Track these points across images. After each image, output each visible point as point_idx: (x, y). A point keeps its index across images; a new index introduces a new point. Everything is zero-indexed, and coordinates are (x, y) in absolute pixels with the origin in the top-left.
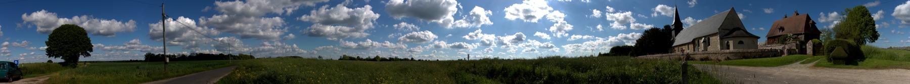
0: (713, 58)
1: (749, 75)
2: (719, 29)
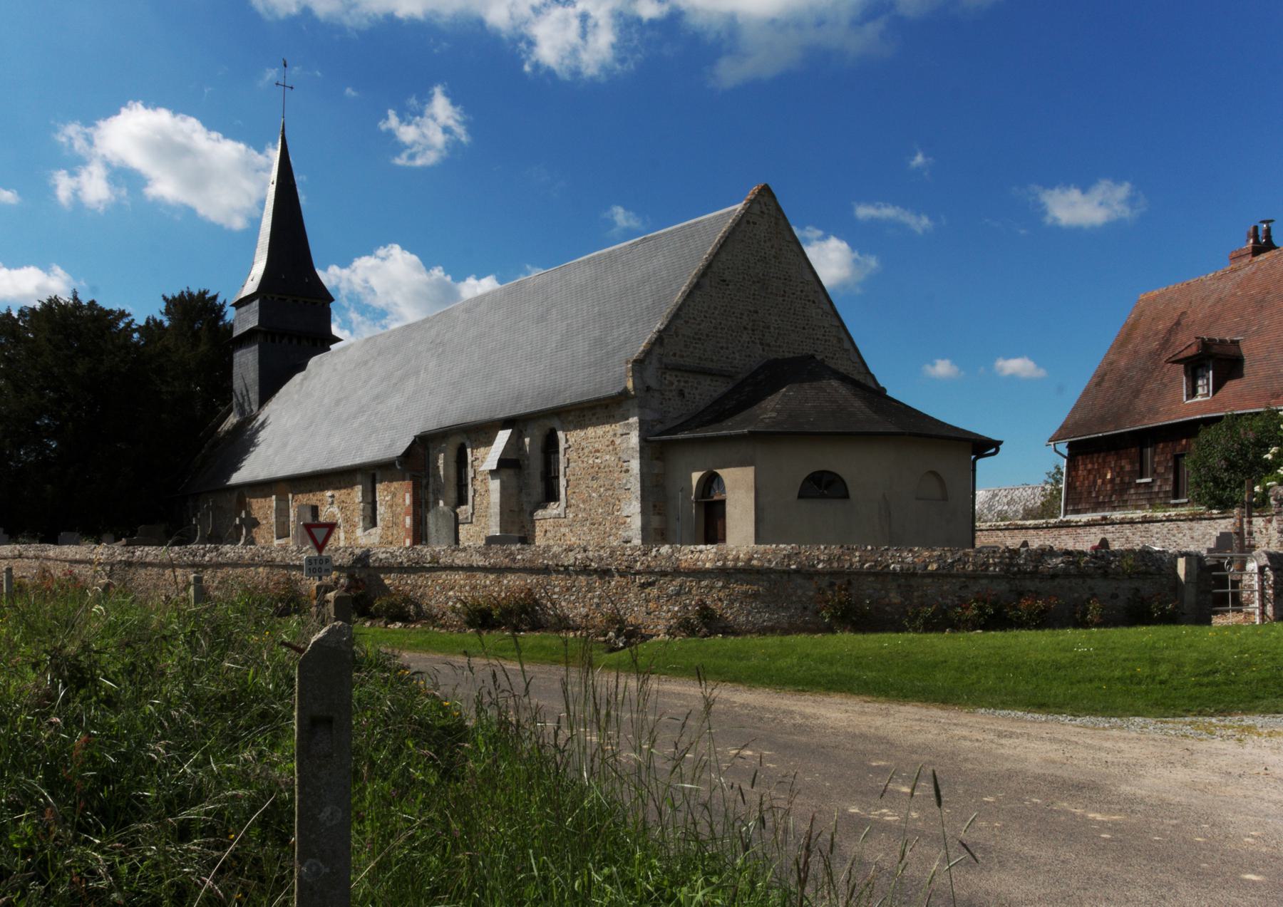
0: (576, 611)
1: (894, 775)
2: (639, 365)
